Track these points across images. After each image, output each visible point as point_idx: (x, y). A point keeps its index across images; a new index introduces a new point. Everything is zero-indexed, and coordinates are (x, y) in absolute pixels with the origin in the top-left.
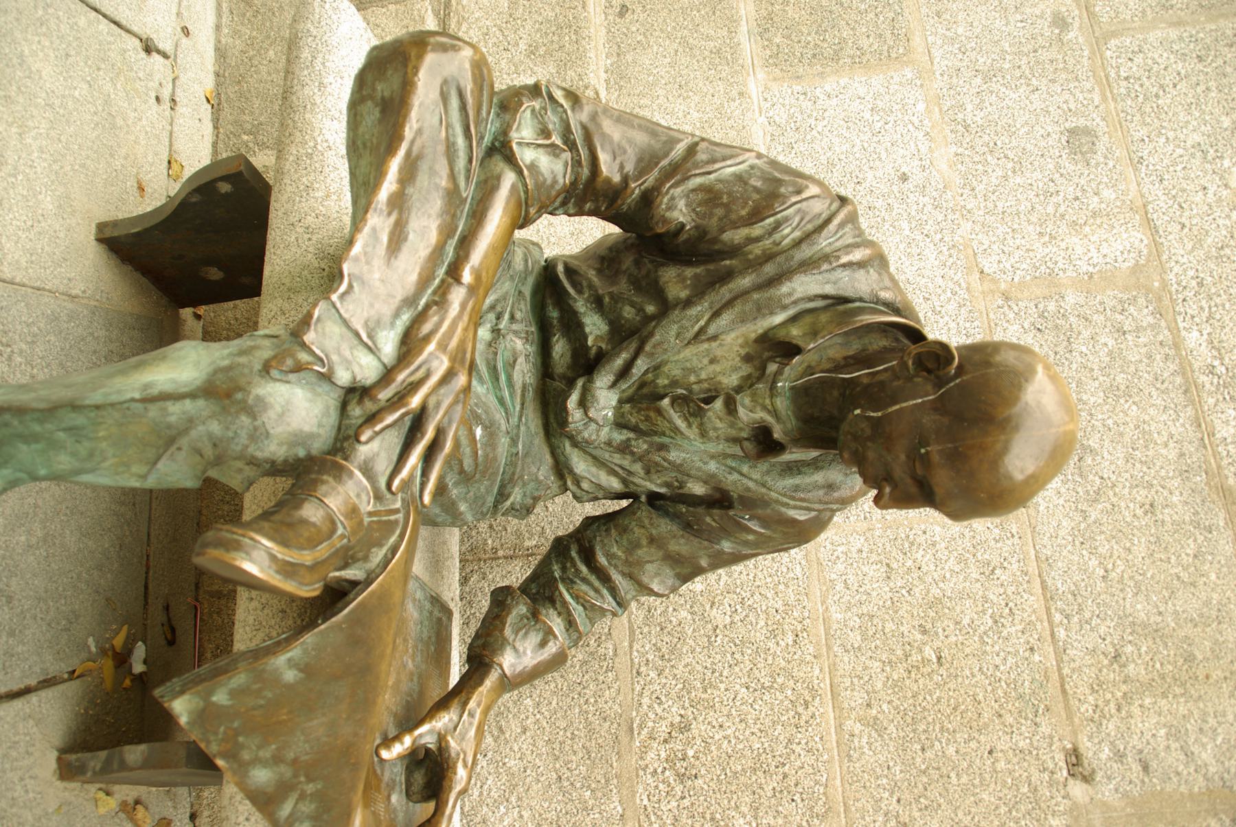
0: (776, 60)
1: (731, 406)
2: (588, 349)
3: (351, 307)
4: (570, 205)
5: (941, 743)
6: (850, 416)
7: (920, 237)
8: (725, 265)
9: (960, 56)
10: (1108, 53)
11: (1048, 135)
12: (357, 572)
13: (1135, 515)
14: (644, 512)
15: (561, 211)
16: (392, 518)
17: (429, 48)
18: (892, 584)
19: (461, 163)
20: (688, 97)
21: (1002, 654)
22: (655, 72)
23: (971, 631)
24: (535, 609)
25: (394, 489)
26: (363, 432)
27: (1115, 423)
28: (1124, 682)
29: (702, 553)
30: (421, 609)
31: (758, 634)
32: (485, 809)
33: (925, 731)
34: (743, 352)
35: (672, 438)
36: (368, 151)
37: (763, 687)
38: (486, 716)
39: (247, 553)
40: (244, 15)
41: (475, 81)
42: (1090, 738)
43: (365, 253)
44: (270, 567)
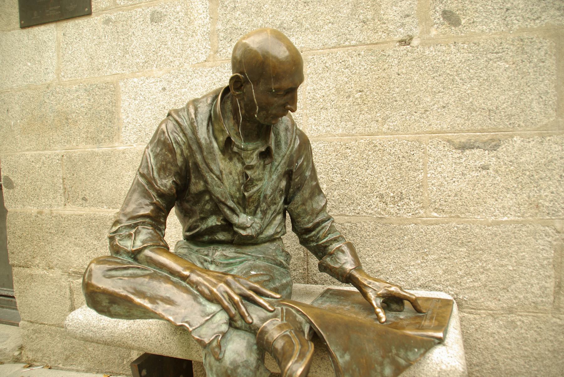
0: (111, 138)
1: (250, 168)
2: (222, 225)
3: (195, 322)
4: (161, 227)
5: (394, 94)
6: (258, 119)
7: (189, 85)
8: (192, 165)
9: (117, 62)
10: (122, 4)
11: (152, 30)
12: (306, 327)
13: (309, 10)
14: (292, 206)
15: (163, 232)
16: (285, 311)
17: (89, 282)
18: (329, 108)
19: (139, 272)
20: (123, 175)
21: (360, 66)
22: (111, 188)
23: (350, 78)
24: (328, 254)
25: (272, 310)
26: (248, 321)
27: (271, 14)
28: (374, 20)
29: (310, 184)
30: (325, 301)
31: (346, 163)
32: (409, 280)
33: (389, 100)
34: (228, 161)
35: (261, 193)
36: (131, 311)
37: (367, 163)
38: (371, 277)
39: (294, 372)
40: (73, 359)
41: (105, 264)
42: (395, 35)
43: (173, 315)
44: (300, 363)
